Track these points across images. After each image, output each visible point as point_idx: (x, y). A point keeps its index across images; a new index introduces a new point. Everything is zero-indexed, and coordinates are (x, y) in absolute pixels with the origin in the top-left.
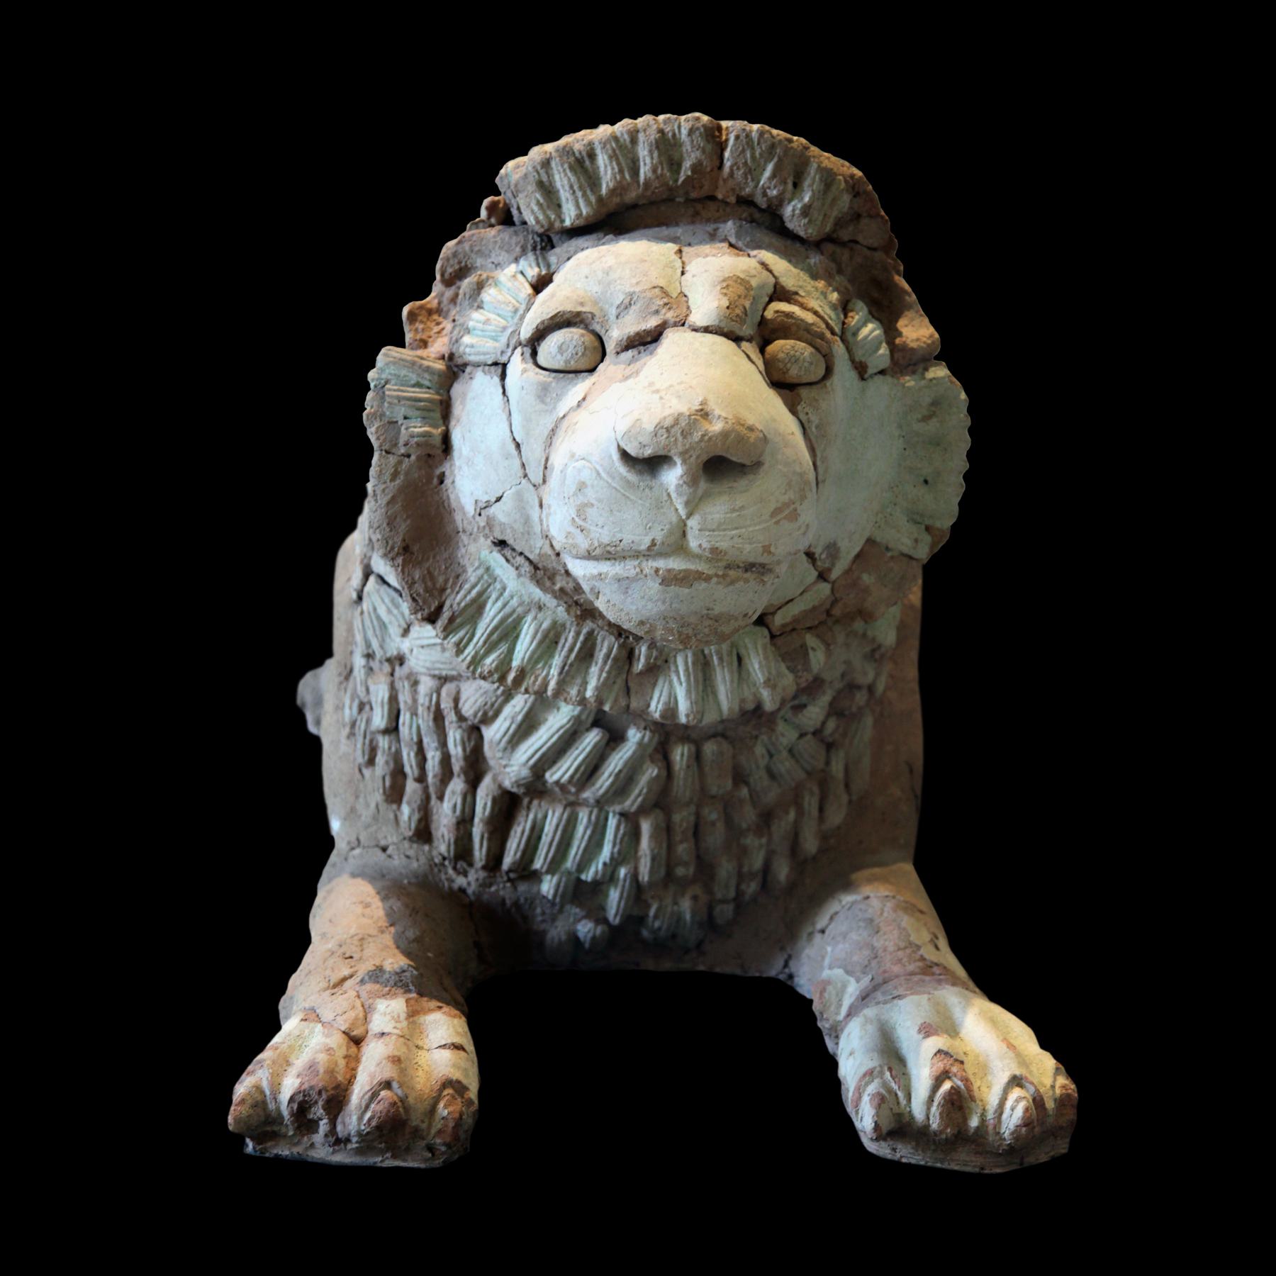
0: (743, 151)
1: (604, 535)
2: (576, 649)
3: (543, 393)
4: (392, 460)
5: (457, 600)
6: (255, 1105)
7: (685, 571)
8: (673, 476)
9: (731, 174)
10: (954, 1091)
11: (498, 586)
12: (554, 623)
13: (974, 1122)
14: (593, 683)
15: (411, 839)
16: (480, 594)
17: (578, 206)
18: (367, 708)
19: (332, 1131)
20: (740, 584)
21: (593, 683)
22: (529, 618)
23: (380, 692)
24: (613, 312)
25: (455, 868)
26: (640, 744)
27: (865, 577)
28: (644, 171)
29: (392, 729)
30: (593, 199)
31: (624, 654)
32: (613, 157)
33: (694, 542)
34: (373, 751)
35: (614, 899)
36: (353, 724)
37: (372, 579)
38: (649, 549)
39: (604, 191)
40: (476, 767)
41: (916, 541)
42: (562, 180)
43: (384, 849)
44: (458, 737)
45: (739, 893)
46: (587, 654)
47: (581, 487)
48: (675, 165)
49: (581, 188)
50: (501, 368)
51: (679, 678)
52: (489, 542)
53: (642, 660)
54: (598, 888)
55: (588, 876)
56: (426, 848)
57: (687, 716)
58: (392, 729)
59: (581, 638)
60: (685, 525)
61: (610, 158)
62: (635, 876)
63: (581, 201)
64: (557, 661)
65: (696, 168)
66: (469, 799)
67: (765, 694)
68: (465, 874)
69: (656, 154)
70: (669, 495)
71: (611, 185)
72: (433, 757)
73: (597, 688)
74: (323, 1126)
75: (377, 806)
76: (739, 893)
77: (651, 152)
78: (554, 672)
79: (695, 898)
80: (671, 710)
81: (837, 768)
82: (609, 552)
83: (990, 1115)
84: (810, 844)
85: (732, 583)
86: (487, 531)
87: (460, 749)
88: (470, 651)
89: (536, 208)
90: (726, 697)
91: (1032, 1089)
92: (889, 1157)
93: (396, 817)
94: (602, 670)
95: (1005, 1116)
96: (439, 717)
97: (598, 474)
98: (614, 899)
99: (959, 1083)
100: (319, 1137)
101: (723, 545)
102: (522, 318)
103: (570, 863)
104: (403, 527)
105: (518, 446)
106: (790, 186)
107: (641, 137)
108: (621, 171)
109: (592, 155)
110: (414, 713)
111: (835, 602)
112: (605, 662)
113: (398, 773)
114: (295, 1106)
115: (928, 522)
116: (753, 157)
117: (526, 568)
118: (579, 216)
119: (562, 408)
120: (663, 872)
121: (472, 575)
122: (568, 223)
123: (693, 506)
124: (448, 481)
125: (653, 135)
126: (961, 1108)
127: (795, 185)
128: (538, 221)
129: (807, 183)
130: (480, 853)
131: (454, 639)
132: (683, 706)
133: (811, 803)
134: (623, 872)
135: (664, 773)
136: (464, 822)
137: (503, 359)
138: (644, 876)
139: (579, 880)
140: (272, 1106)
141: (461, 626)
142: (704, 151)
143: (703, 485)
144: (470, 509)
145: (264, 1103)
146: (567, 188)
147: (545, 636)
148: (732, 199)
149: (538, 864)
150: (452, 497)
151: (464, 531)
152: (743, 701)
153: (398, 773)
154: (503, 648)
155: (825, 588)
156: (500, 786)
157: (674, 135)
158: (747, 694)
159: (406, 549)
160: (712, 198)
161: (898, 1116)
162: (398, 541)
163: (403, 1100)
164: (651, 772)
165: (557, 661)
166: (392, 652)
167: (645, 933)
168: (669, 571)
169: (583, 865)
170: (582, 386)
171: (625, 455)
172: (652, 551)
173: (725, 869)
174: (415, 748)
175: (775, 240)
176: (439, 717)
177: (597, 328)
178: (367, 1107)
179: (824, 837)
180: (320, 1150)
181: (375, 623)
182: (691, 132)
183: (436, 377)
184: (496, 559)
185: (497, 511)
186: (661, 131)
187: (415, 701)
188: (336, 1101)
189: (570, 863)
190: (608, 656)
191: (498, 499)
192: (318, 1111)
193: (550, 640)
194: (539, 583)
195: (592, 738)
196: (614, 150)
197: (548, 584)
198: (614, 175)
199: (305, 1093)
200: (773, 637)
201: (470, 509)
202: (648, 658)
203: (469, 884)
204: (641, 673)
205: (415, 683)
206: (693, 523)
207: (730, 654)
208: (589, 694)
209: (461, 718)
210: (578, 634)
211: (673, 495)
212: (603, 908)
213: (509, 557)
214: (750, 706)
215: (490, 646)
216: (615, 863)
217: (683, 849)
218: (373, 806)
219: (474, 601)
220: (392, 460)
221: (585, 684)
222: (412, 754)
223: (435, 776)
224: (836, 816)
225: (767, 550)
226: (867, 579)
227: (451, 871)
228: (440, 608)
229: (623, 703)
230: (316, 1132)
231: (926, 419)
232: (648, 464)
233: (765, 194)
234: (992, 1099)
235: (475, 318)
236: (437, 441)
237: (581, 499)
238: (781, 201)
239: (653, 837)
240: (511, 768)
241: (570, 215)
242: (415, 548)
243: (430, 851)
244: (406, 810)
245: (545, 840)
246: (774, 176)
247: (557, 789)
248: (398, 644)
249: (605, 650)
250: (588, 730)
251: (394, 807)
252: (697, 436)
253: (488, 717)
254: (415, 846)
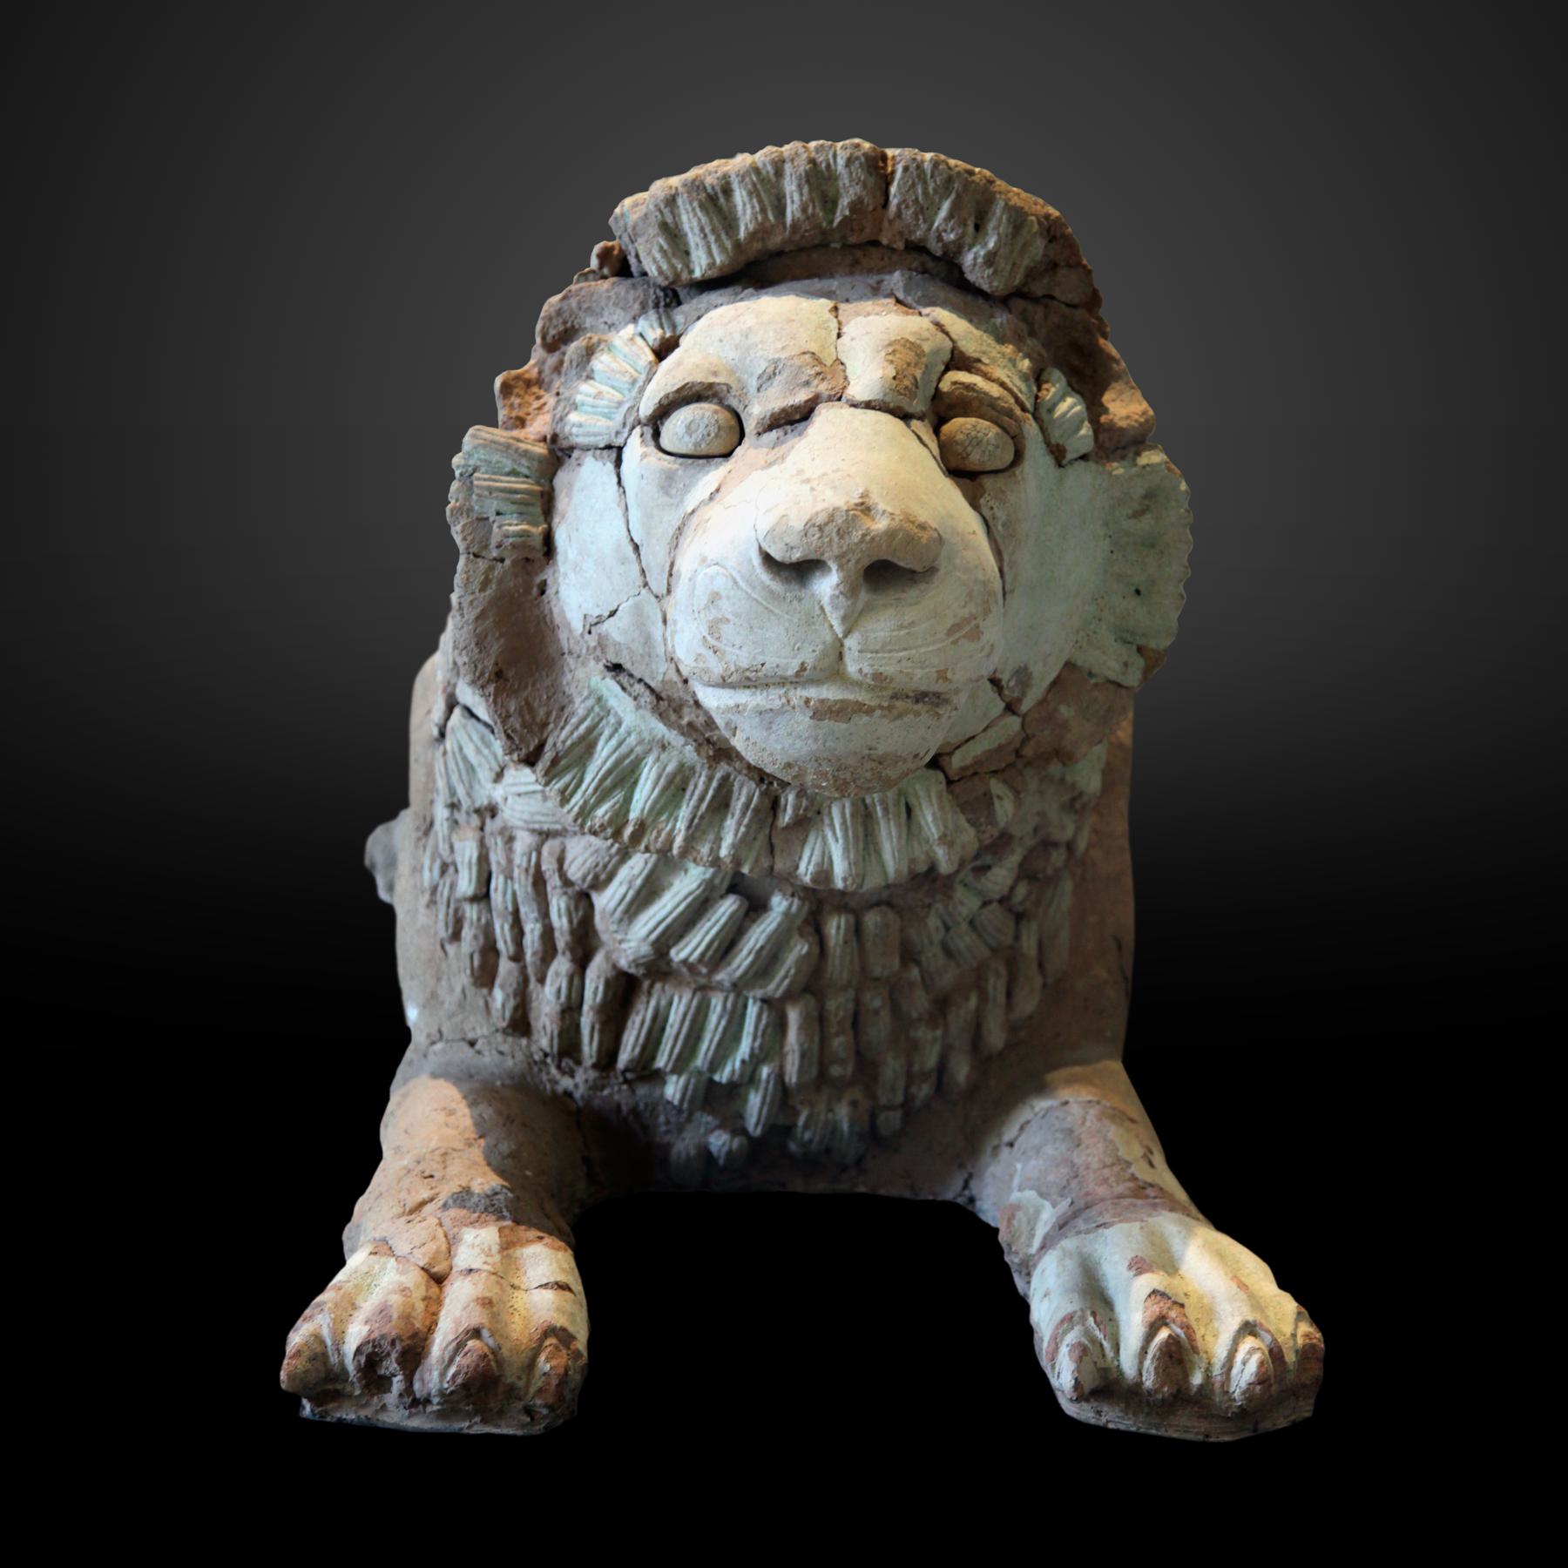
0: (913, 186)
1: (742, 658)
2: (708, 798)
3: (668, 482)
4: (482, 565)
5: (561, 737)
6: (313, 1358)
7: (842, 701)
8: (826, 585)
9: (899, 214)
10: (1173, 1341)
11: (612, 720)
12: (681, 766)
13: (1197, 1379)
14: (728, 840)
15: (505, 1032)
16: (590, 730)
17: (710, 253)
18: (451, 869)
19: (409, 1389)
20: (909, 718)
21: (728, 840)
22: (650, 760)
23: (467, 851)
24: (753, 383)
25: (559, 1067)
26: (787, 914)
27: (1063, 709)
28: (792, 210)
29: (482, 896)
30: (728, 244)
31: (767, 803)
32: (753, 192)
33: (853, 666)
34: (458, 923)
35: (755, 1105)
36: (434, 890)
37: (457, 711)
38: (797, 674)
39: (742, 234)
40: (584, 942)
41: (1126, 664)
42: (691, 221)
43: (472, 1044)
44: (563, 906)
45: (909, 1098)
46: (721, 804)
47: (714, 598)
48: (829, 203)
49: (714, 231)
50: (616, 453)
51: (834, 833)
52: (601, 666)
53: (789, 810)
54: (735, 1091)
55: (723, 1076)
56: (524, 1042)
57: (845, 879)
58: (482, 896)
59: (715, 784)
60: (842, 645)
61: (750, 194)
62: (780, 1076)
63: (714, 248)
64: (684, 812)
65: (855, 206)
66: (576, 981)
67: (941, 853)
68: (572, 1074)
69: (806, 190)
70: (822, 608)
71: (751, 227)
72: (532, 930)
73: (733, 846)
74: (398, 1384)
75: (463, 990)
76: (909, 1098)
77: (800, 187)
78: (681, 825)
79: (854, 1104)
80: (824, 873)
81: (1029, 944)
82: (748, 679)
83: (1217, 1371)
84: (996, 1038)
85: (900, 716)
86: (598, 652)
87: (565, 921)
88: (577, 800)
89: (658, 256)
90: (892, 857)
91: (1268, 1338)
92: (1093, 1421)
93: (487, 1004)
94: (739, 824)
95: (1234, 1372)
96: (539, 882)
97: (735, 582)
98: (755, 1105)
99: (1179, 1331)
100: (391, 1398)
101: (889, 670)
102: (642, 390)
103: (700, 1060)
104: (495, 648)
105: (636, 548)
106: (971, 229)
107: (788, 168)
108: (763, 210)
109: (727, 191)
110: (509, 877)
111: (1026, 739)
112: (743, 814)
113: (489, 950)
114: (363, 1359)
115: (1141, 641)
116: (925, 192)
117: (647, 697)
118: (712, 265)
119: (691, 502)
120: (814, 1071)
121: (580, 707)
122: (697, 274)
123: (851, 622)
124: (550, 592)
125: (803, 165)
126: (1181, 1362)
127: (977, 227)
128: (661, 272)
129: (991, 225)
130: (589, 1048)
131: (558, 785)
132: (840, 868)
133: (996, 986)
134: (765, 1071)
135: (816, 950)
136: (570, 1010)
137: (619, 442)
138: (792, 1076)
139: (711, 1082)
140: (334, 1359)
141: (566, 769)
142: (865, 186)
143: (864, 596)
144: (578, 625)
145: (325, 1355)
146: (697, 231)
147: (670, 782)
148: (900, 245)
149: (661, 1062)
150: (556, 611)
151: (570, 653)
152: (913, 861)
153: (489, 950)
154: (618, 796)
155: (1014, 723)
156: (614, 966)
157: (828, 165)
158: (918, 852)
159: (499, 675)
160: (875, 243)
161: (1104, 1372)
162: (489, 664)
163: (495, 1352)
164: (800, 949)
165: (684, 812)
166: (482, 801)
167: (793, 1147)
168: (822, 701)
169: (716, 1063)
170: (715, 475)
171: (767, 559)
172: (802, 677)
173: (891, 1067)
174: (510, 919)
175: (953, 295)
176: (539, 882)
177: (734, 403)
178: (451, 1360)
179: (1013, 1029)
180: (393, 1413)
181: (461, 765)
182: (849, 162)
183: (536, 464)
184: (609, 687)
185: (611, 628)
186: (813, 161)
187: (510, 861)
188: (413, 1352)
189: (700, 1060)
190: (747, 806)
191: (612, 614)
192: (391, 1365)
193: (675, 787)
194: (662, 716)
195: (727, 907)
196: (754, 185)
197: (673, 717)
198: (754, 215)
199: (375, 1344)
200: (949, 782)
201: (578, 625)
202: (796, 808)
203: (576, 1086)
204: (788, 827)
205: (510, 840)
206: (852, 643)
207: (897, 803)
208: (724, 852)
209: (567, 883)
210: (710, 779)
211: (828, 609)
212: (741, 1116)
213: (626, 685)
214: (922, 868)
215: (602, 794)
216: (755, 1060)
217: (840, 1044)
218: (458, 990)
219: (582, 738)
220: (482, 565)
221: (718, 840)
222: (507, 927)
223: (534, 954)
224: (1027, 1003)
225: (942, 675)
226: (1065, 711)
227: (554, 1071)
228: (541, 747)
229: (766, 864)
230: (389, 1390)
231: (1137, 515)
232: (796, 571)
233: (940, 238)
234: (1220, 1351)
235: (584, 391)
236: (537, 542)
237: (714, 613)
238: (960, 247)
239: (803, 1028)
240: (629, 943)
241: (700, 264)
242: (510, 674)
243: (528, 1046)
244: (498, 995)
245: (670, 1032)
246: (951, 216)
247: (684, 970)
248: (489, 792)
249: (743, 799)
250: (722, 897)
251: (485, 991)
252: (856, 536)
253: (600, 881)
254: (510, 1039)
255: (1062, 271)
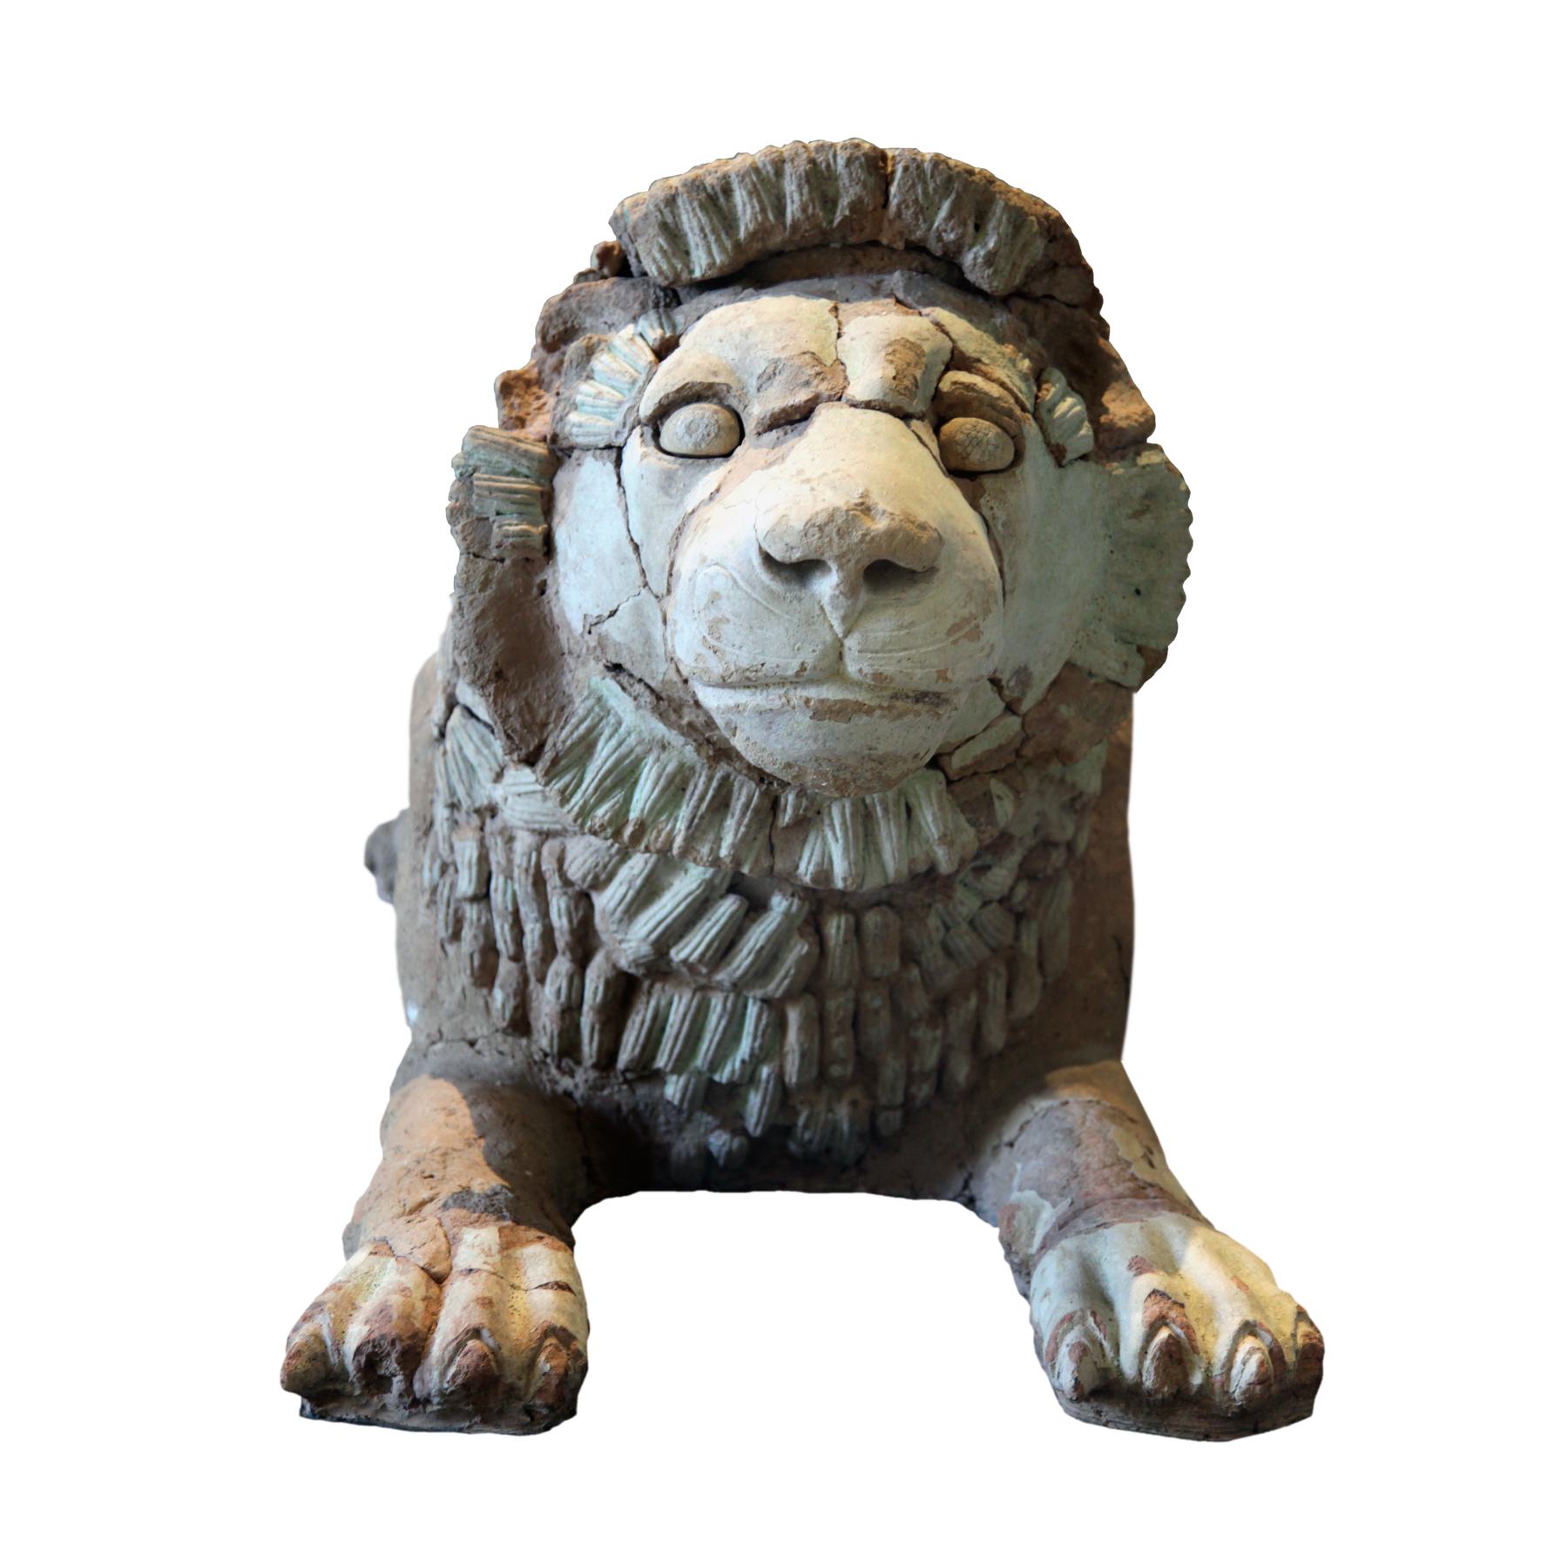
0: (913, 186)
1: (742, 658)
2: (708, 798)
3: (668, 482)
4: (482, 565)
5: (561, 737)
6: (313, 1358)
7: (842, 701)
8: (826, 585)
9: (899, 214)
11: (612, 720)
12: (681, 766)
13: (1197, 1379)
14: (728, 840)
15: (505, 1032)
16: (590, 730)
17: (710, 253)
18: (451, 869)
19: (409, 1389)
20: (909, 718)
21: (728, 840)
22: (650, 760)
23: (467, 851)
24: (753, 383)
25: (559, 1067)
26: (787, 914)
27: (1063, 709)
28: (792, 210)
29: (482, 896)
30: (728, 244)
31: (767, 803)
32: (753, 192)
33: (853, 666)
34: (458, 923)
35: (755, 1105)
36: (434, 890)
37: (457, 711)
38: (797, 674)
39: (742, 234)
40: (584, 942)
41: (1126, 664)
43: (472, 1044)
44: (563, 906)
45: (909, 1098)
46: (721, 804)
47: (714, 598)
48: (829, 203)
49: (714, 231)
50: (616, 453)
51: (834, 833)
53: (789, 810)
54: (735, 1091)
55: (723, 1076)
56: (524, 1042)
57: (845, 879)
58: (482, 896)
59: (715, 784)
60: (842, 645)
61: (750, 194)
62: (780, 1076)
63: (714, 248)
64: (684, 812)
65: (855, 206)
66: (576, 981)
67: (941, 853)
68: (572, 1074)
69: (806, 190)
70: (822, 608)
71: (751, 227)
72: (532, 930)
73: (733, 846)
74: (398, 1384)
75: (463, 990)
76: (909, 1098)
77: (800, 187)
78: (681, 825)
79: (854, 1104)
80: (824, 873)
81: (1029, 944)
82: (748, 679)
83: (1217, 1371)
84: (996, 1038)
85: (900, 716)
86: (598, 652)
87: (565, 921)
88: (577, 800)
89: (658, 256)
90: (892, 857)
93: (487, 1004)
94: (739, 824)
96: (539, 882)
97: (735, 582)
98: (755, 1105)
101: (889, 670)
102: (642, 390)
103: (700, 1060)
104: (495, 648)
105: (636, 548)
106: (971, 229)
107: (788, 168)
108: (763, 210)
110: (509, 877)
111: (1026, 739)
112: (743, 814)
113: (489, 950)
114: (363, 1359)
115: (1141, 641)
116: (925, 192)
117: (647, 697)
118: (712, 265)
119: (691, 502)
120: (814, 1071)
121: (580, 707)
122: (697, 274)
123: (851, 622)
124: (550, 592)
127: (977, 227)
128: (661, 272)
129: (991, 225)
130: (589, 1048)
131: (558, 785)
132: (840, 868)
133: (996, 986)
134: (765, 1071)
135: (816, 950)
136: (570, 1010)
137: (619, 442)
138: (792, 1076)
139: (711, 1082)
140: (334, 1359)
141: (566, 769)
142: (865, 186)
143: (864, 596)
144: (578, 625)
145: (325, 1355)
146: (697, 231)
147: (670, 782)
148: (900, 245)
149: (661, 1062)
150: (556, 611)
151: (570, 653)
152: (913, 861)
153: (489, 950)
154: (618, 796)
155: (1014, 723)
156: (614, 966)
157: (828, 165)
158: (918, 852)
159: (499, 675)
160: (875, 243)
162: (489, 664)
163: (495, 1352)
164: (800, 949)
165: (684, 812)
166: (482, 801)
167: (793, 1147)
168: (822, 701)
169: (716, 1063)
170: (715, 475)
171: (767, 559)
172: (802, 677)
173: (891, 1067)
174: (510, 919)
175: (953, 295)
176: (539, 882)
177: (734, 403)
178: (451, 1360)
179: (1013, 1029)
181: (461, 765)
183: (536, 464)
184: (609, 687)
185: (611, 628)
187: (510, 861)
188: (413, 1352)
189: (700, 1060)
190: (747, 806)
191: (612, 614)
192: (391, 1365)
194: (662, 716)
195: (727, 907)
196: (754, 185)
197: (673, 717)
198: (754, 215)
199: (375, 1344)
200: (949, 782)
201: (578, 625)
202: (796, 808)
203: (576, 1086)
204: (788, 827)
205: (510, 840)
206: (852, 643)
207: (897, 803)
208: (724, 852)
209: (567, 883)
210: (710, 779)
211: (828, 609)
212: (741, 1116)
213: (626, 685)
214: (922, 868)
215: (602, 794)
216: (755, 1060)
217: (840, 1044)
218: (458, 990)
219: (582, 738)
220: (482, 565)
221: (718, 840)
222: (507, 927)
223: (534, 954)
224: (1027, 1003)
225: (942, 675)
226: (1065, 711)
227: (554, 1071)
228: (541, 747)
229: (766, 864)
230: (389, 1390)
231: (1137, 515)
232: (796, 571)
233: (940, 238)
235: (584, 391)
236: (537, 542)
237: (714, 613)
238: (960, 247)
239: (803, 1028)
240: (629, 943)
241: (700, 264)
242: (510, 674)
243: (528, 1046)
244: (498, 995)
245: (670, 1032)
246: (951, 216)
247: (684, 970)
248: (489, 792)
249: (743, 799)
250: (722, 897)
251: (485, 991)
252: (856, 536)
253: (600, 881)
254: (510, 1039)
255: (1062, 271)
